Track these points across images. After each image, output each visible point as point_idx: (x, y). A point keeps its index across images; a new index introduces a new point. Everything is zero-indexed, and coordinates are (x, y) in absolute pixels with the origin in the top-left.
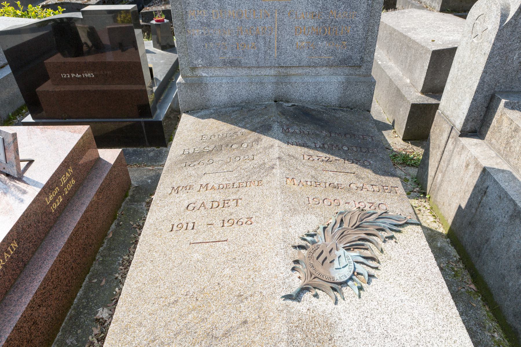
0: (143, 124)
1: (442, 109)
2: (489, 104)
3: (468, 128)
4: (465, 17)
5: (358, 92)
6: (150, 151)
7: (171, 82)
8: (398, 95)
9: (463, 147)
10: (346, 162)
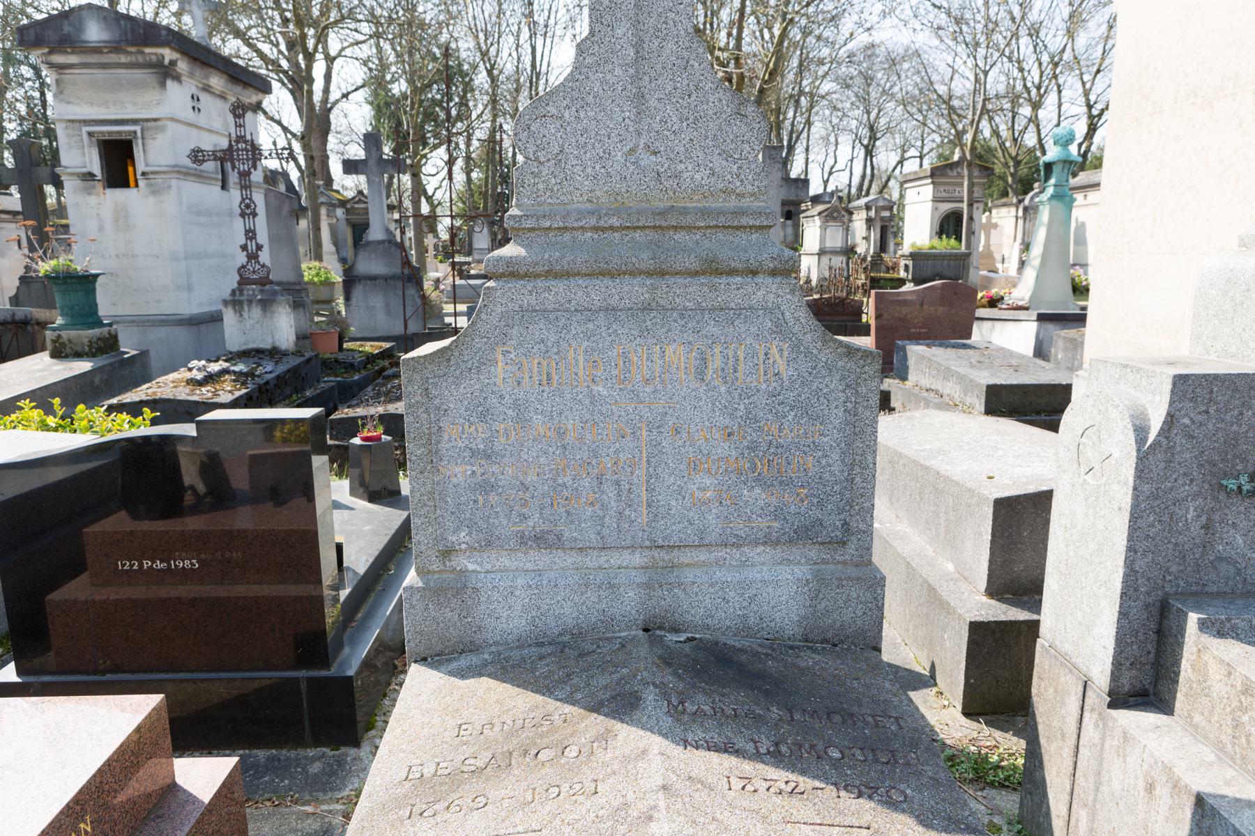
0: (303, 686)
1: (1048, 636)
2: (1160, 624)
3: (1126, 684)
4: (1054, 427)
5: (845, 603)
6: (313, 760)
7: (385, 577)
8: (934, 600)
9: (1126, 737)
10: (843, 793)
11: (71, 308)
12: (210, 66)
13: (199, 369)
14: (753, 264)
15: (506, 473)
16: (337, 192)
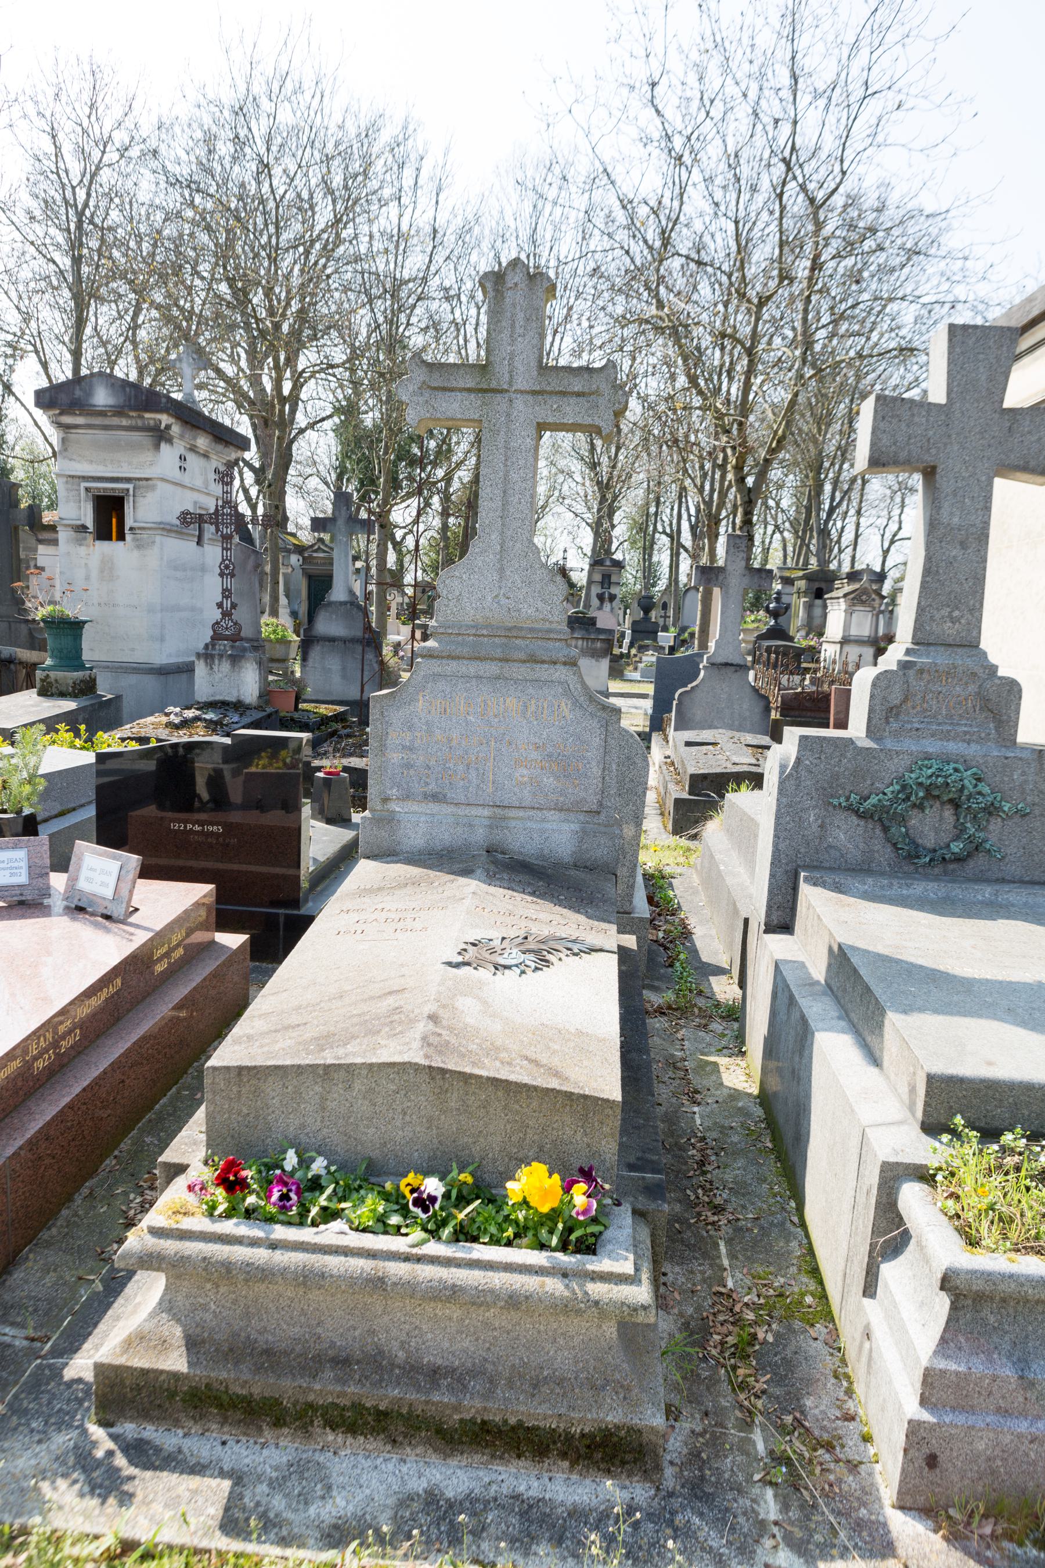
0: (282, 920)
11: (61, 651)
12: (198, 428)
13: (176, 714)
14: (554, 658)
15: (419, 759)
16: (294, 535)
